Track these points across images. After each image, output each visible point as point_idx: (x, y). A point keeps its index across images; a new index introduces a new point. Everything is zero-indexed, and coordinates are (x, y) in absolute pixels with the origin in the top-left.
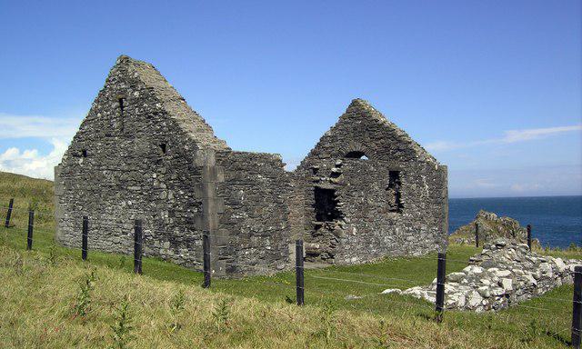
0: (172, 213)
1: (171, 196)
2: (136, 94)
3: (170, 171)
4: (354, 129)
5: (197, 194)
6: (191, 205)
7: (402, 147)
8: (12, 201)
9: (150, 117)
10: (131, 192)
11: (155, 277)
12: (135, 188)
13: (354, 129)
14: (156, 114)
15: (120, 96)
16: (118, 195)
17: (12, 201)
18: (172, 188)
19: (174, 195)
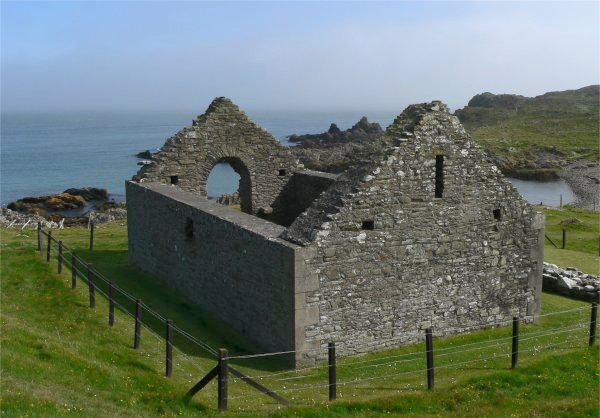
0: (504, 278)
1: (504, 261)
2: (464, 152)
3: (505, 236)
4: (228, 132)
5: (533, 255)
6: (525, 266)
7: (281, 153)
8: (332, 394)
9: (483, 180)
10: (452, 265)
11: (268, 370)
12: (459, 260)
13: (228, 132)
14: (491, 177)
15: (439, 152)
16: (432, 272)
17: (332, 394)
18: (506, 253)
19: (508, 261)
